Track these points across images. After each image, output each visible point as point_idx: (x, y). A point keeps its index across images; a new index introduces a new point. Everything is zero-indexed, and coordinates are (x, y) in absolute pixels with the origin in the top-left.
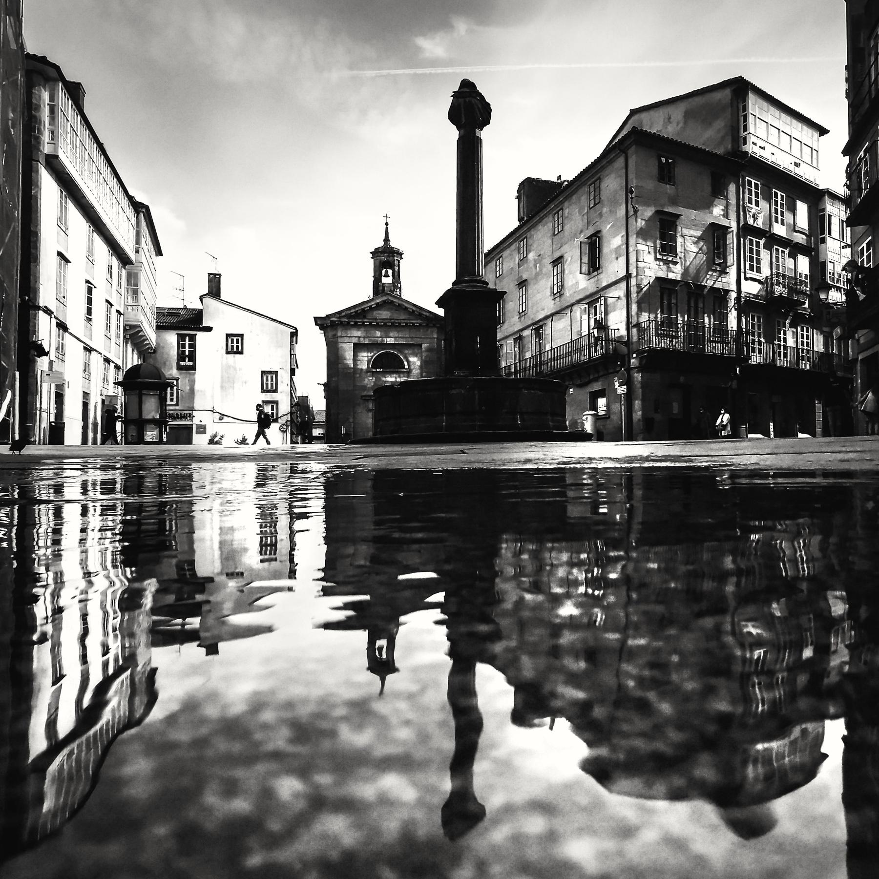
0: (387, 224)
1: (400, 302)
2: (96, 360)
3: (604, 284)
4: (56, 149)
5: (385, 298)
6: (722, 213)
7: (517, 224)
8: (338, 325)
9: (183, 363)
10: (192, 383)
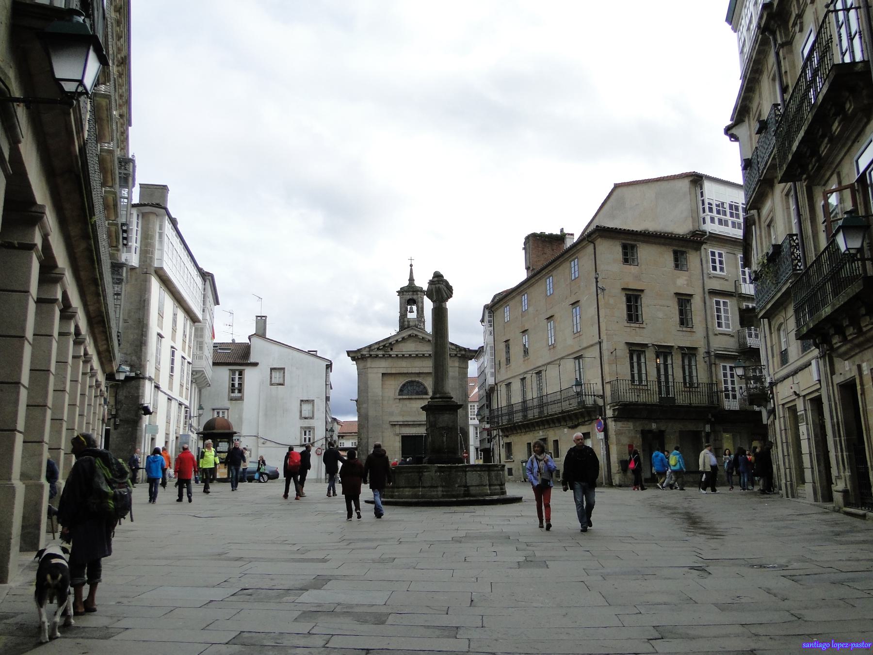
0: (411, 266)
1: (424, 336)
2: (174, 405)
3: (585, 345)
4: (162, 263)
5: (410, 332)
6: (685, 283)
7: (522, 275)
8: (368, 357)
9: (233, 395)
10: (241, 411)
